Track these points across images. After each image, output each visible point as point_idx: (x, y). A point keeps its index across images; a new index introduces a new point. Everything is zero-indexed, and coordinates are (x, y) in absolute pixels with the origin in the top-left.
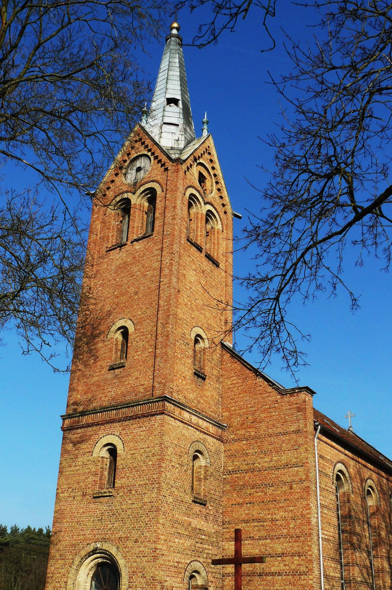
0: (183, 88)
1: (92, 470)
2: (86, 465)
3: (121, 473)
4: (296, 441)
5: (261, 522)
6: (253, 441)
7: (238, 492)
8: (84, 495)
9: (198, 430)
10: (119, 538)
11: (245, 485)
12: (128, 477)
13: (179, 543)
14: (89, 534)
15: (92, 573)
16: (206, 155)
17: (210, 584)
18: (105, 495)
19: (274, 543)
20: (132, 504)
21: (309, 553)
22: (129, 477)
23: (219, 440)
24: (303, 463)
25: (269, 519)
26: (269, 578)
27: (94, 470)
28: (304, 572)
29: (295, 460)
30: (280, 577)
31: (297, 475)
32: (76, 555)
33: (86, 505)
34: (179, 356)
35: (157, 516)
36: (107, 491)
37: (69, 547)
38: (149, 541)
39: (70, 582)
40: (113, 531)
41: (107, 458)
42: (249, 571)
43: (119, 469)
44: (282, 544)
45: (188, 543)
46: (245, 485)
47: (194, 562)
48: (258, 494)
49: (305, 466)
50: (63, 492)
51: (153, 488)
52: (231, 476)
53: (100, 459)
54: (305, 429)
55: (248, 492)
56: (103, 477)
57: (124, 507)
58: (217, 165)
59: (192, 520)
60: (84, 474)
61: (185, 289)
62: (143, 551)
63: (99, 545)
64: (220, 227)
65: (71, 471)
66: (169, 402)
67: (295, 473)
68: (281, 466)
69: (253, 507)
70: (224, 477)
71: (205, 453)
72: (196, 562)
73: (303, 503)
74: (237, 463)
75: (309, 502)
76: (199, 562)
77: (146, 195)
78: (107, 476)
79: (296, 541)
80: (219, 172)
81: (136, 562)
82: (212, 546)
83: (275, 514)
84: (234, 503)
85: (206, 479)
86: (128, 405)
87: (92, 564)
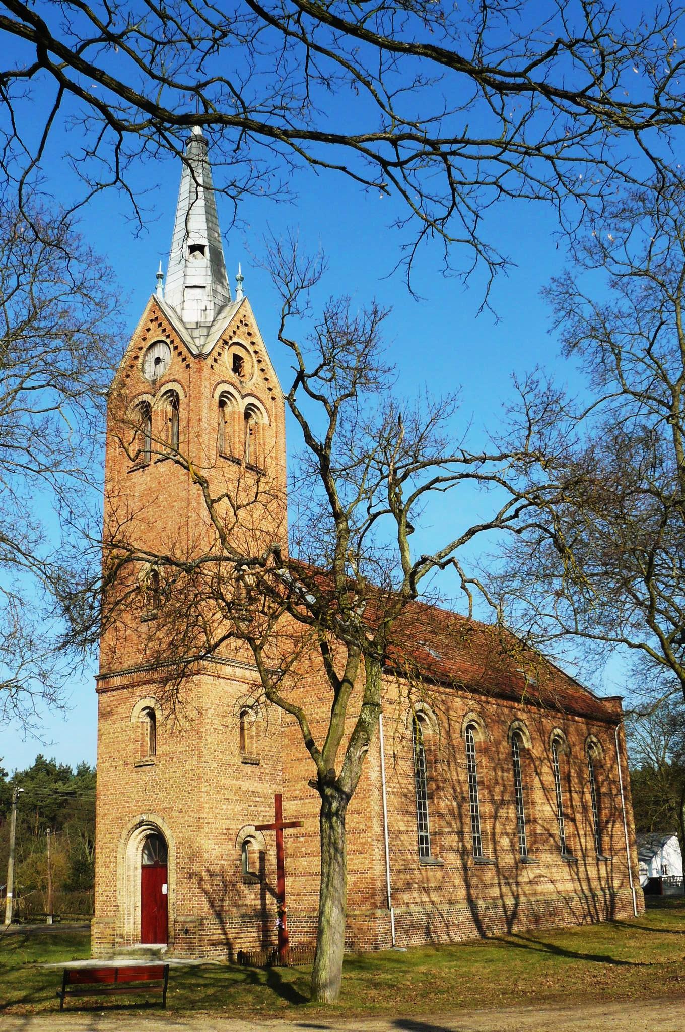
0: (210, 225)
6: (310, 689)
8: (126, 764)
16: (243, 329)
17: (269, 847)
39: (119, 856)
45: (238, 808)
50: (104, 762)
53: (139, 724)
57: (166, 776)
58: (258, 339)
63: (144, 817)
64: (266, 420)
77: (169, 397)
87: (141, 836)
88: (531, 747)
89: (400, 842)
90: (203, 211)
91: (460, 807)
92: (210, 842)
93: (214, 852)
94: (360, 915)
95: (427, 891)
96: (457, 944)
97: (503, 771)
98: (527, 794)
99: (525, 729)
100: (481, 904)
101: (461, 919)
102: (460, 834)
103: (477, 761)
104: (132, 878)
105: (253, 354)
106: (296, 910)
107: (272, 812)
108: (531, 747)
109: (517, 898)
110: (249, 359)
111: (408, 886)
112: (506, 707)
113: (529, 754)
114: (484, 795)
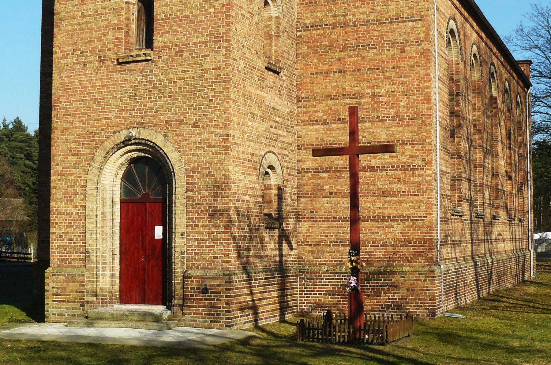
1: (112, 22)
2: (102, 14)
3: (164, 26)
5: (357, 98)
7: (321, 55)
8: (102, 60)
10: (167, 122)
11: (332, 45)
12: (175, 33)
13: (253, 127)
14: (116, 118)
15: (121, 172)
18: (139, 59)
19: (375, 127)
20: (185, 71)
21: (428, 140)
22: (178, 31)
24: (422, 16)
25: (368, 93)
27: (116, 22)
28: (420, 166)
29: (409, 11)
30: (384, 173)
31: (412, 33)
32: (96, 147)
33: (107, 75)
35: (228, 88)
36: (141, 53)
37: (84, 137)
38: (216, 125)
39: (90, 186)
40: (157, 112)
41: (134, 4)
42: (338, 165)
43: (159, 20)
44: (388, 128)
45: (262, 127)
46: (332, 45)
47: (268, 154)
48: (352, 59)
49: (424, 21)
51: (219, 48)
52: (308, 32)
53: (124, 6)
55: (337, 55)
56: (130, 33)
57: (172, 76)
59: (265, 95)
60: (98, 28)
62: (208, 140)
65: (76, 24)
67: (408, 30)
68: (387, 19)
69: (344, 77)
70: (298, 34)
72: (271, 154)
73: (421, 72)
74: (319, 14)
75: (429, 71)
76: (274, 153)
78: (135, 31)
81: (197, 155)
82: (287, 131)
83: (378, 87)
87: (123, 160)
94: (412, 273)
104: (109, 217)
106: (313, 264)
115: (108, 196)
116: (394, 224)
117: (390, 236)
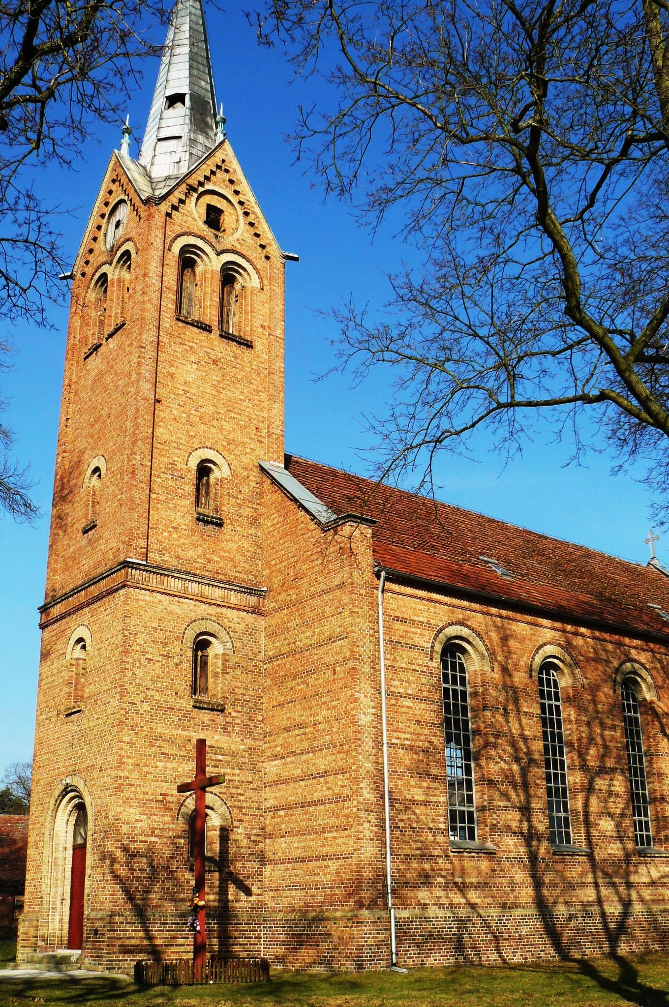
4: (340, 601)
9: (202, 602)
23: (253, 612)
26: (312, 809)
30: (323, 807)
34: (162, 498)
53: (74, 662)
54: (350, 580)
57: (91, 724)
58: (244, 186)
61: (173, 396)
64: (255, 282)
66: (136, 569)
70: (265, 667)
71: (222, 634)
79: (339, 753)
80: (248, 195)
84: (275, 703)
85: (225, 672)
86: (95, 581)
88: (655, 699)
89: (413, 817)
90: (187, 58)
91: (524, 772)
92: (132, 810)
93: (139, 825)
94: (342, 918)
95: (462, 888)
96: (514, 968)
97: (603, 726)
98: (650, 762)
99: (644, 673)
100: (561, 910)
101: (524, 931)
102: (526, 811)
103: (563, 715)
105: (237, 206)
107: (192, 765)
108: (655, 699)
109: (627, 904)
110: (232, 211)
111: (426, 879)
112: (611, 642)
113: (653, 709)
114: (573, 760)
115: (61, 840)
116: (330, 863)
117: (328, 877)
